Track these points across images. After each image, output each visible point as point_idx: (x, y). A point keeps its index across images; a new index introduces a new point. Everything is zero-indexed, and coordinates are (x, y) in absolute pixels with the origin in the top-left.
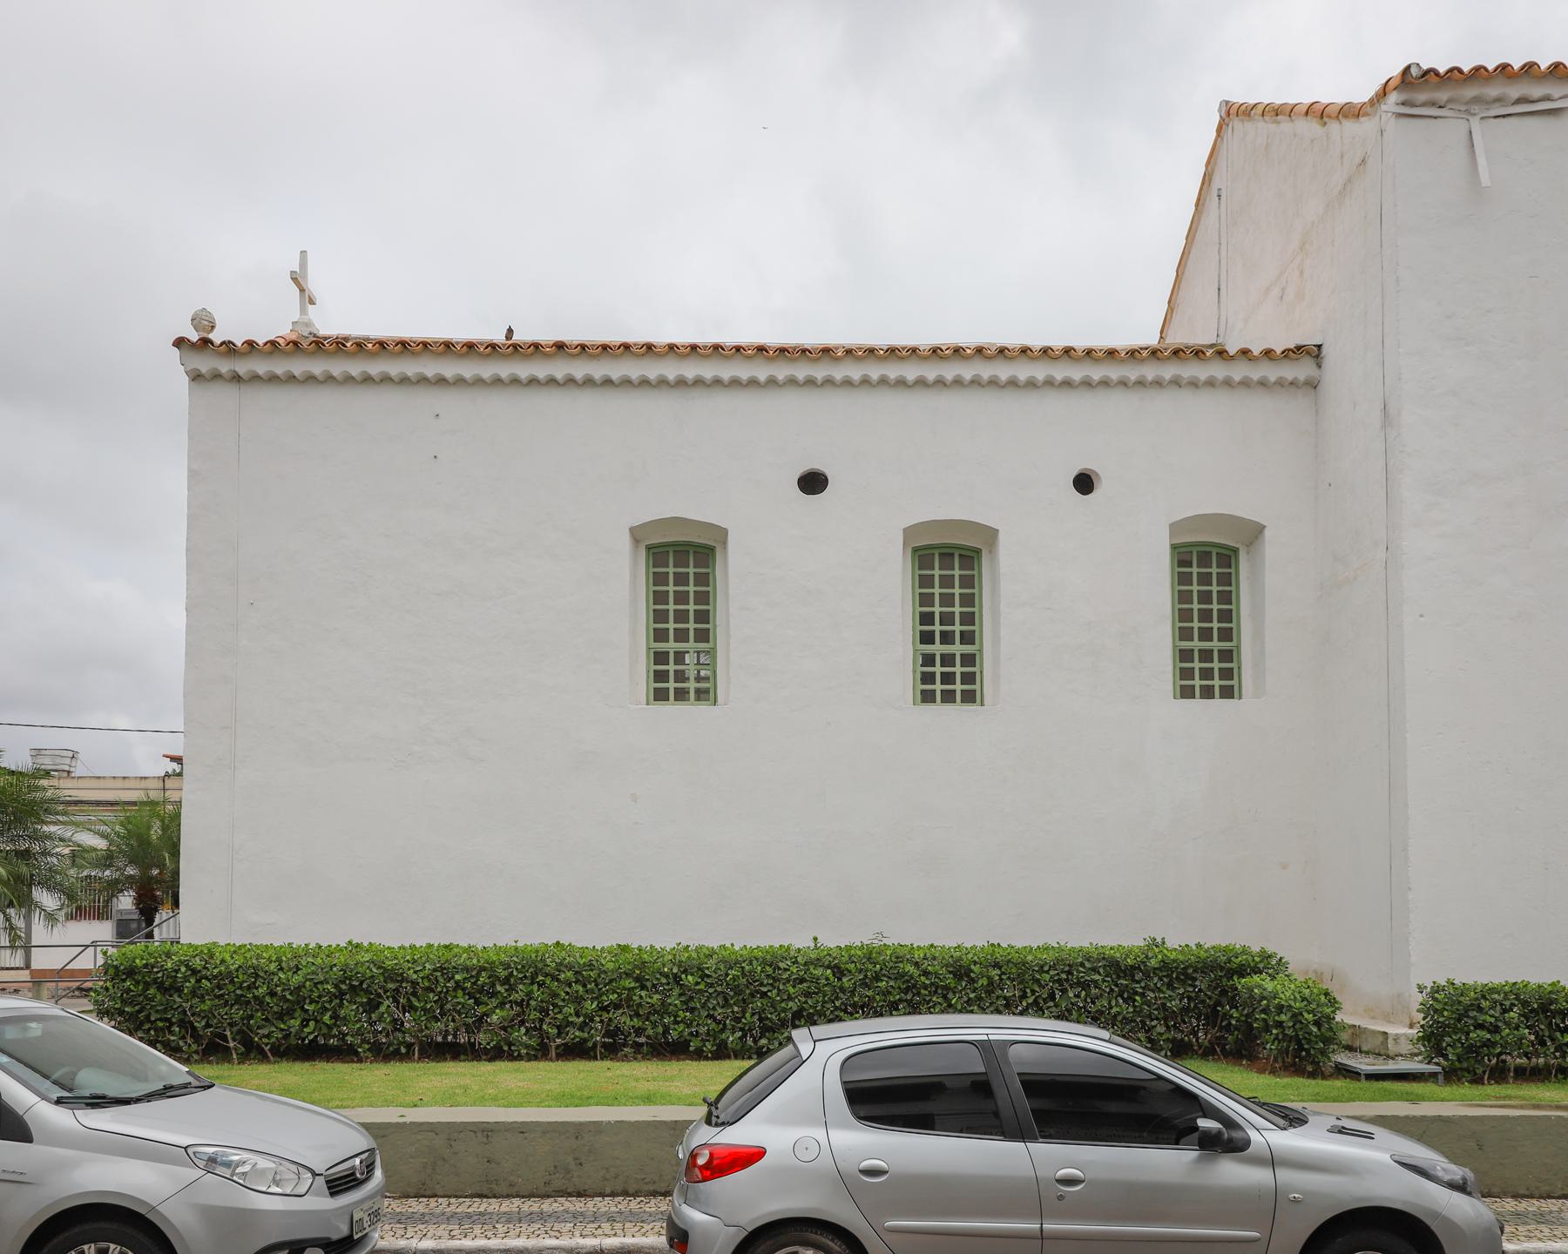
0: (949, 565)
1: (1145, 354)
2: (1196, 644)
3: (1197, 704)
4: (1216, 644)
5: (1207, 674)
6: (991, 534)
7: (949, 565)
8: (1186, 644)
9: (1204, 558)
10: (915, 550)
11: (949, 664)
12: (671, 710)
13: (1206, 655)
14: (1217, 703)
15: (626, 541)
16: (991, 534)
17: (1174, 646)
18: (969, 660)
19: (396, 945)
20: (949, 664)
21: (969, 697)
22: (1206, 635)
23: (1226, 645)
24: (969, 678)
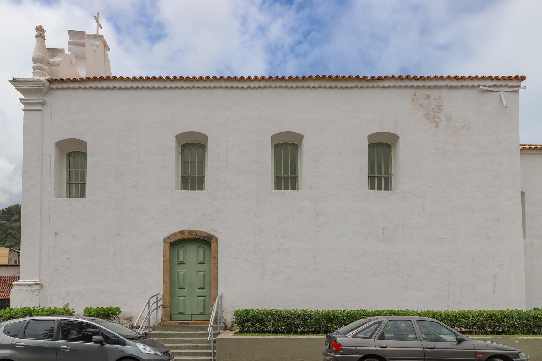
11: (286, 177)
20: (286, 177)
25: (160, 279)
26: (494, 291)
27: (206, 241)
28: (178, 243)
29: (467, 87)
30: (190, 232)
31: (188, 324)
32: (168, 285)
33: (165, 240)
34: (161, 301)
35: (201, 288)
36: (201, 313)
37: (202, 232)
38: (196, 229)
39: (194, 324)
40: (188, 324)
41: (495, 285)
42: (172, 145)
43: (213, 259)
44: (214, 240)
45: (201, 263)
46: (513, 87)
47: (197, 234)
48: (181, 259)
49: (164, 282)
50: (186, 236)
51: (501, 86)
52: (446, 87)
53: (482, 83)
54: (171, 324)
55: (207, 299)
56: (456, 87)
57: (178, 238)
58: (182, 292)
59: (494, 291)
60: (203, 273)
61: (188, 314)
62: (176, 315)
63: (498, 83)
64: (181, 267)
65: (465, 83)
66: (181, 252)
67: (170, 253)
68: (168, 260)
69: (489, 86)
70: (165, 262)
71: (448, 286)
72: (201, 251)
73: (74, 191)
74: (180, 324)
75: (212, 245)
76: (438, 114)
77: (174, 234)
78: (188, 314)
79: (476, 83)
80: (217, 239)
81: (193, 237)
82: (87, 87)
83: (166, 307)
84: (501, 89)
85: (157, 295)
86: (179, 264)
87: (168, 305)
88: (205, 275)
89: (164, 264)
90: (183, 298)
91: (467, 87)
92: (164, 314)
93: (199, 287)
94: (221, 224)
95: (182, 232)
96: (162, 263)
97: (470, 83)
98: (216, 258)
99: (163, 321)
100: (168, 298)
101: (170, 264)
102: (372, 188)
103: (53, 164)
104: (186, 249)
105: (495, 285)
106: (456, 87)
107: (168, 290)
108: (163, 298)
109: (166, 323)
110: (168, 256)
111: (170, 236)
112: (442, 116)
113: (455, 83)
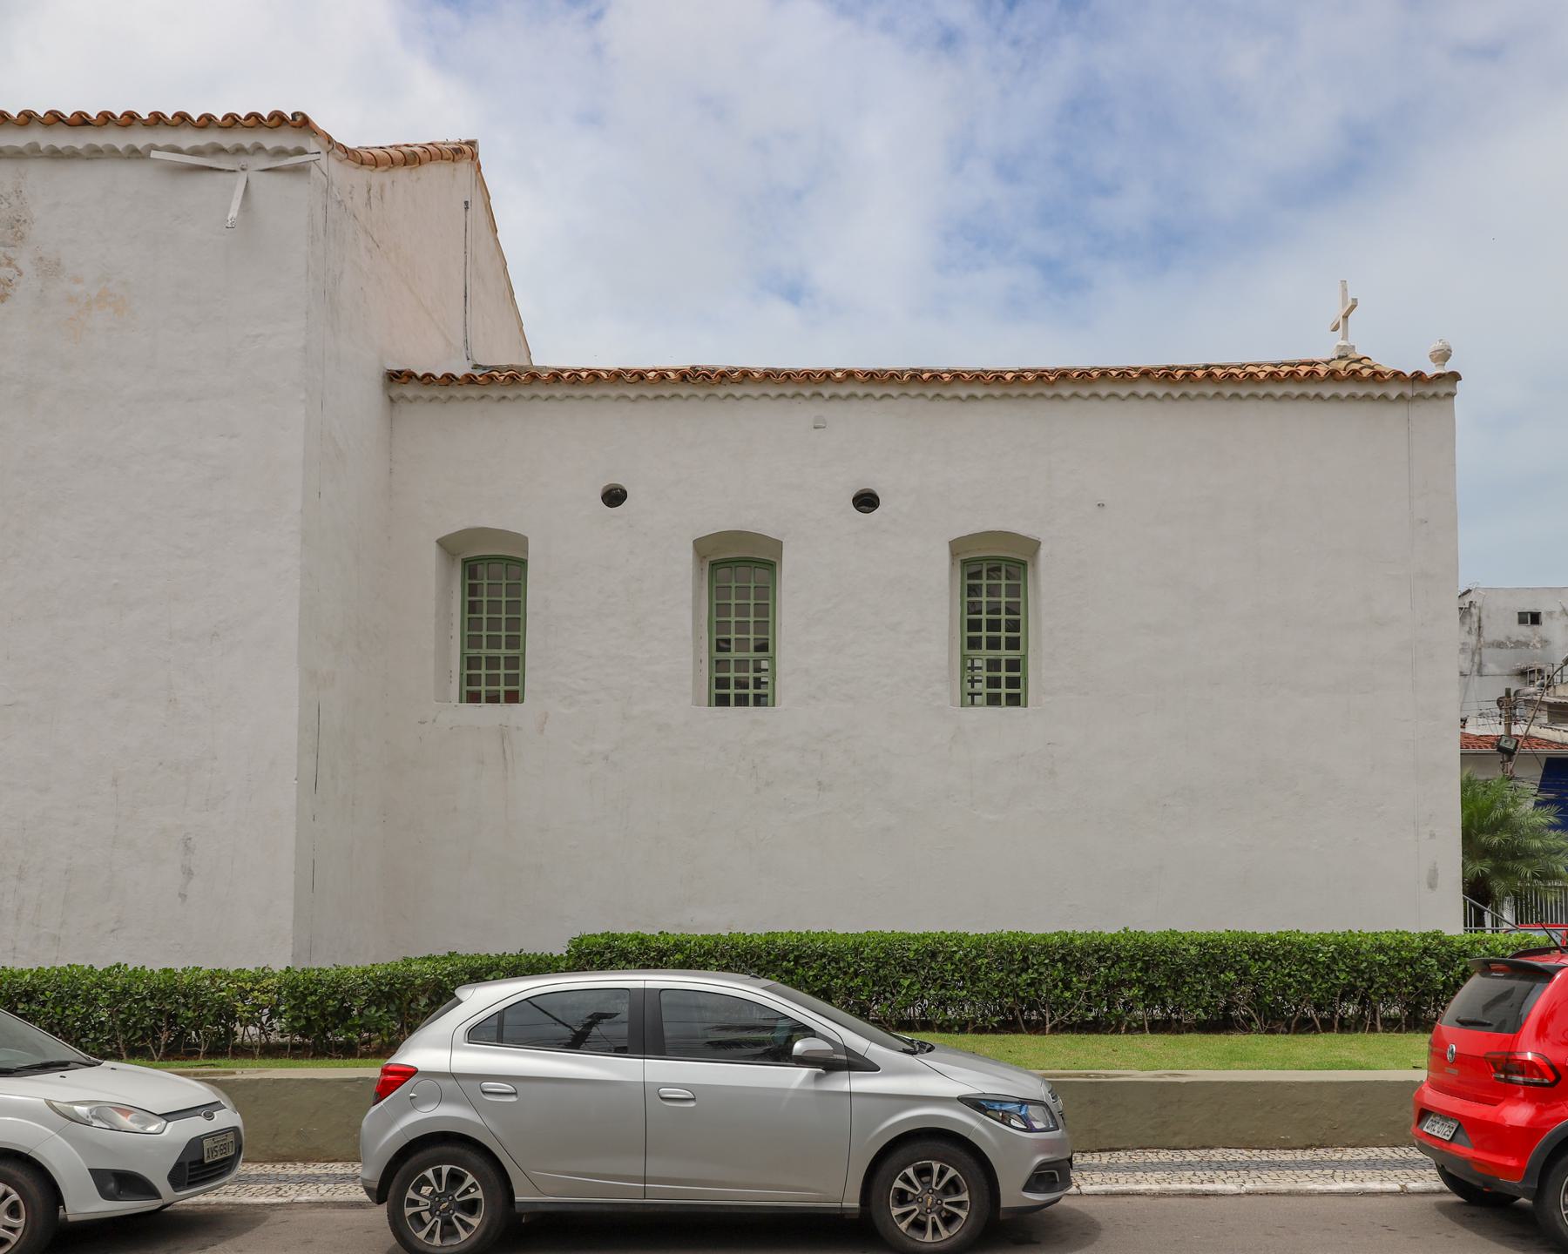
0: (739, 575)
1: (1030, 377)
2: (485, 651)
3: (732, 711)
4: (503, 652)
5: (493, 680)
6: (1034, 546)
7: (739, 575)
8: (474, 652)
9: (994, 571)
10: (964, 562)
11: (739, 670)
12: (733, 714)
13: (493, 662)
14: (751, 711)
15: (688, 555)
16: (1034, 546)
17: (462, 654)
18: (1014, 665)
19: (863, 931)
20: (739, 670)
21: (1014, 700)
22: (494, 642)
23: (511, 652)
24: (1014, 682)
26: (183, 896)
29: (113, 153)
41: (189, 873)
42: (684, 563)
46: (281, 152)
51: (239, 150)
52: (33, 153)
53: (163, 138)
56: (72, 155)
59: (183, 896)
63: (228, 140)
65: (100, 139)
69: (196, 152)
71: (20, 878)
76: (10, 254)
79: (140, 139)
82: (226, 147)
84: (244, 160)
91: (113, 153)
97: (118, 140)
102: (970, 698)
105: (189, 873)
106: (72, 155)
112: (24, 260)
113: (63, 139)
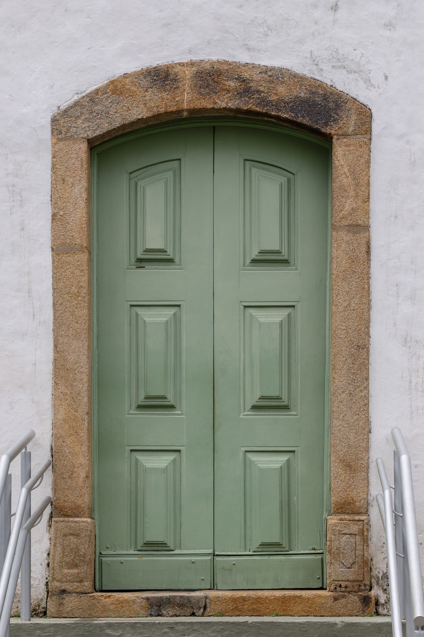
25: (37, 354)
27: (298, 130)
28: (146, 135)
30: (210, 77)
31: (203, 607)
32: (83, 387)
33: (61, 124)
34: (48, 477)
35: (269, 405)
36: (270, 548)
37: (276, 75)
38: (243, 57)
39: (237, 606)
40: (203, 607)
43: (344, 236)
44: (350, 123)
45: (269, 260)
47: (246, 90)
48: (154, 237)
49: (61, 369)
50: (187, 98)
54: (105, 612)
55: (300, 467)
57: (139, 112)
58: (157, 428)
60: (277, 317)
61: (194, 548)
62: (128, 562)
64: (153, 282)
66: (154, 194)
67: (89, 200)
68: (79, 238)
70: (60, 249)
72: (268, 188)
73: (126, 326)
74: (157, 607)
75: (340, 152)
77: (116, 88)
78: (194, 548)
80: (365, 115)
81: (223, 102)
83: (72, 512)
85: (24, 445)
86: (141, 262)
87: (84, 501)
88: (288, 327)
89: (57, 267)
90: (163, 461)
92: (64, 556)
93: (253, 398)
94: (389, 26)
95: (161, 77)
96: (45, 259)
98: (361, 229)
99: (57, 593)
100: (80, 459)
101: (90, 260)
103: (156, 458)
104: (178, 176)
107: (83, 410)
108: (56, 461)
109: (71, 602)
110: (78, 214)
111: (93, 98)
